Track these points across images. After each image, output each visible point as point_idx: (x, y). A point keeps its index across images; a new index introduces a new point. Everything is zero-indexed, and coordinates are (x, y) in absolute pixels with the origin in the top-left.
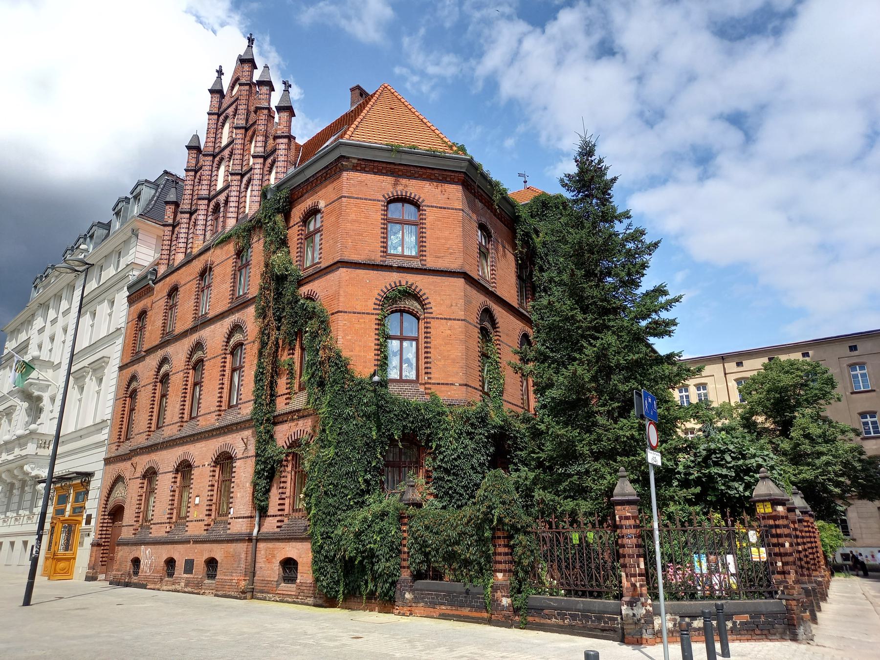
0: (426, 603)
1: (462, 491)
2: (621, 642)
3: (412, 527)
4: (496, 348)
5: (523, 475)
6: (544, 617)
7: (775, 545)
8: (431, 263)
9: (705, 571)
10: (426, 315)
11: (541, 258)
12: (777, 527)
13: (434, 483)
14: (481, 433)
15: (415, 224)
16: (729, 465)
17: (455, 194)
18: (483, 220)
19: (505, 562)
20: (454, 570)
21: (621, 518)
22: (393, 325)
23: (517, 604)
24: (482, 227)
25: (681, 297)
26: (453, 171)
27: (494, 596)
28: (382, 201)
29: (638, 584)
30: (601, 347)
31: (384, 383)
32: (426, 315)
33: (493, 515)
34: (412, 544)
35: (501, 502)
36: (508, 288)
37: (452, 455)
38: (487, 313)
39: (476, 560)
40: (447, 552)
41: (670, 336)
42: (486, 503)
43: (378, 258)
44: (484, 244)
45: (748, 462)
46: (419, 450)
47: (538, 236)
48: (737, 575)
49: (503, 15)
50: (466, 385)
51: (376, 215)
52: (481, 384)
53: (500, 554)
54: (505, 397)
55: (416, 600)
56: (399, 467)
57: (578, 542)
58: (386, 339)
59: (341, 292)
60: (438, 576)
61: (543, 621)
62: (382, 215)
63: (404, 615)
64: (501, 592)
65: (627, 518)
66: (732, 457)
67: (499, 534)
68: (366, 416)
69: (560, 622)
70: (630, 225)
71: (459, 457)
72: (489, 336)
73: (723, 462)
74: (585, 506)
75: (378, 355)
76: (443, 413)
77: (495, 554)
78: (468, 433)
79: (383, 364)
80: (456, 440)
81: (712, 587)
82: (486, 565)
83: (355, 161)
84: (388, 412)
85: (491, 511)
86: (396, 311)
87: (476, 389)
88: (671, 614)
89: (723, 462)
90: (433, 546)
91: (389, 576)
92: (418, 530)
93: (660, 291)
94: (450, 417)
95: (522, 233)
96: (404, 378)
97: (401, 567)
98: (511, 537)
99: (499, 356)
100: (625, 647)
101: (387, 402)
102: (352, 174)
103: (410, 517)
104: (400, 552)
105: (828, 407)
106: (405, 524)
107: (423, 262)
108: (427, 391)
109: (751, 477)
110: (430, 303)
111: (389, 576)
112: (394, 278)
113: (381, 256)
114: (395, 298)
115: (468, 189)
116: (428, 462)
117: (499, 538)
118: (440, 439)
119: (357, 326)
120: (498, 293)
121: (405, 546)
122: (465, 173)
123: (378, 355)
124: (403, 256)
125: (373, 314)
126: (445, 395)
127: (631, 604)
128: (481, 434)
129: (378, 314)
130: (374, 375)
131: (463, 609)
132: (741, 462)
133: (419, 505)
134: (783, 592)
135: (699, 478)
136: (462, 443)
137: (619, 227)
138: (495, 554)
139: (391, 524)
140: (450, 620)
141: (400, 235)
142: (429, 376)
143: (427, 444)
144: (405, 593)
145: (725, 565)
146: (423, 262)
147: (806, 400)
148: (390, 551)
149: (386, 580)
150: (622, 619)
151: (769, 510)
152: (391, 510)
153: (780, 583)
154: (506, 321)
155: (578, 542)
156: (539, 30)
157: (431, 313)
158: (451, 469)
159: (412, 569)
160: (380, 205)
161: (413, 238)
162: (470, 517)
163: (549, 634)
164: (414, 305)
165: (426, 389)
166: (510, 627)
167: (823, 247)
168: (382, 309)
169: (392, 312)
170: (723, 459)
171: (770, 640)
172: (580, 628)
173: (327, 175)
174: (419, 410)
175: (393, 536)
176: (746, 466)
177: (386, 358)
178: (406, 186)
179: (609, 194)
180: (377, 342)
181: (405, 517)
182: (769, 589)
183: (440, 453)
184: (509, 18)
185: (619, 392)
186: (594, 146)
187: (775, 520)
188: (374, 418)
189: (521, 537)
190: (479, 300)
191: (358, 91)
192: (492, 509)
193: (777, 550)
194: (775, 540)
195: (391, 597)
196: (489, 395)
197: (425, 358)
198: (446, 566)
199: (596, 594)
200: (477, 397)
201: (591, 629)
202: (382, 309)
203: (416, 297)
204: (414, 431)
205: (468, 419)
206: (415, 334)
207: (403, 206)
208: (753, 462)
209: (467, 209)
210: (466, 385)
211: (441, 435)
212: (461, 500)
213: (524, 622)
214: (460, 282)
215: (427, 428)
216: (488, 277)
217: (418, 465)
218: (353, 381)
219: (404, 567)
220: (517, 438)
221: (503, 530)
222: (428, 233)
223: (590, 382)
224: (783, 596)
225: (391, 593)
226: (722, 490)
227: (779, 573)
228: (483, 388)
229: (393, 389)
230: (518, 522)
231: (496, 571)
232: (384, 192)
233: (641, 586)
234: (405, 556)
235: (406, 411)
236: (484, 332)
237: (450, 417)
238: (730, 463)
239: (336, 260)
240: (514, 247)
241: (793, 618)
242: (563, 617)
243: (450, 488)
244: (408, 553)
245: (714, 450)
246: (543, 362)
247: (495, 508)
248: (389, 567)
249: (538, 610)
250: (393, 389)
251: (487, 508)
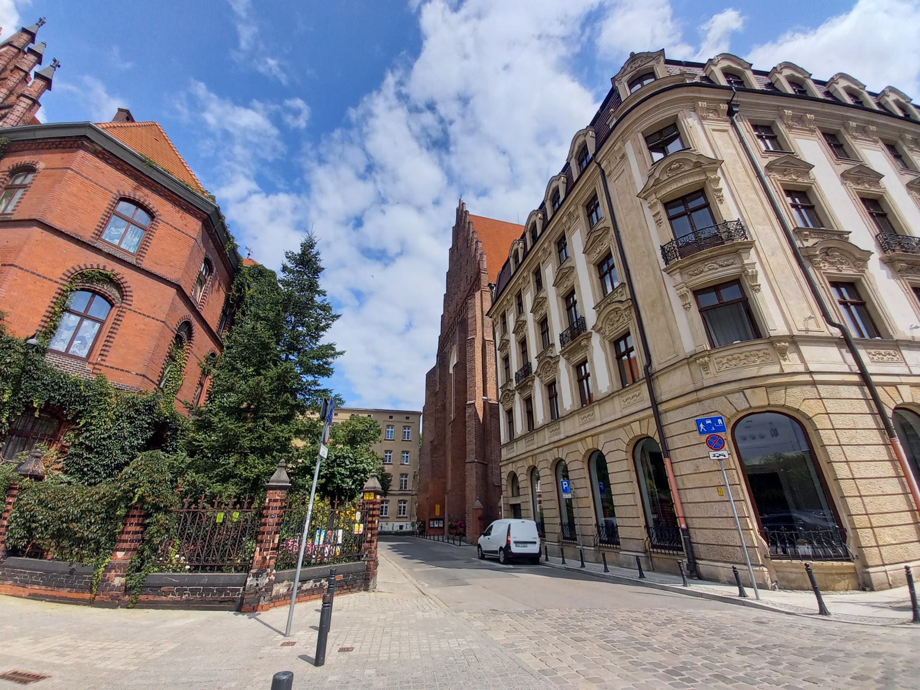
1: (101, 470)
2: (237, 611)
3: (21, 500)
4: (185, 355)
6: (159, 595)
7: (369, 522)
9: (321, 543)
10: (123, 305)
11: (246, 306)
14: (145, 420)
15: (144, 229)
16: (347, 467)
17: (194, 226)
18: (210, 257)
24: (207, 261)
25: (344, 352)
26: (198, 208)
27: (105, 576)
29: (268, 557)
30: (285, 370)
33: (135, 494)
34: (16, 517)
35: (149, 482)
36: (212, 316)
38: (187, 325)
39: (94, 539)
41: (329, 377)
43: (87, 237)
44: (204, 273)
45: (358, 466)
46: (60, 424)
47: (249, 290)
50: (144, 376)
51: (103, 203)
52: (159, 379)
53: (128, 533)
54: (178, 396)
56: (28, 438)
58: (64, 310)
59: (25, 249)
61: (157, 598)
64: (116, 572)
65: (276, 501)
66: (350, 462)
67: (135, 512)
69: (177, 598)
71: (109, 437)
73: (343, 465)
76: (107, 394)
77: (122, 532)
78: (129, 417)
79: (50, 331)
80: (112, 421)
81: (323, 555)
84: (35, 379)
85: (133, 489)
87: (153, 382)
88: (288, 580)
89: (343, 465)
90: (43, 522)
92: (28, 504)
93: (330, 347)
94: (113, 399)
95: (238, 282)
98: (148, 515)
99: (186, 362)
100: (240, 616)
101: (38, 369)
102: (89, 156)
103: (22, 489)
105: (374, 445)
106: (14, 496)
107: (139, 261)
108: (95, 371)
109: (359, 476)
110: (132, 296)
112: (101, 261)
113: (92, 237)
114: (92, 278)
116: (67, 437)
117: (134, 516)
118: (92, 417)
122: (208, 215)
126: (113, 380)
127: (256, 575)
128: (143, 420)
129: (64, 285)
130: (33, 337)
133: (39, 478)
134: (367, 555)
136: (119, 425)
137: (318, 299)
138: (122, 532)
142: (103, 358)
145: (336, 537)
146: (139, 261)
147: (366, 439)
150: (244, 589)
151: (372, 498)
154: (201, 339)
157: (130, 305)
158: (96, 447)
160: (110, 197)
162: (104, 494)
163: (161, 611)
164: (114, 293)
167: (377, 368)
168: (71, 282)
169: (83, 290)
170: (344, 462)
172: (198, 602)
173: (60, 144)
176: (357, 468)
177: (55, 327)
179: (318, 275)
182: (359, 554)
183: (87, 430)
186: (316, 243)
187: (374, 505)
190: (184, 312)
191: (125, 115)
192: (136, 488)
194: (370, 519)
196: (163, 391)
200: (151, 389)
201: (209, 602)
202: (71, 282)
203: (118, 286)
204: (62, 404)
205: (134, 405)
206: (102, 317)
207: (137, 209)
209: (199, 241)
210: (144, 376)
212: (95, 478)
216: (199, 299)
217: (52, 439)
221: (141, 508)
223: (267, 393)
224: (367, 559)
226: (338, 483)
228: (160, 384)
229: (49, 359)
230: (162, 502)
233: (271, 558)
235: (59, 383)
236: (178, 338)
237: (113, 399)
238: (348, 465)
239: (32, 217)
240: (229, 289)
242: (181, 592)
243: (87, 465)
245: (340, 456)
246: (230, 371)
247: (140, 486)
249: (155, 588)
250: (49, 359)
251: (130, 486)
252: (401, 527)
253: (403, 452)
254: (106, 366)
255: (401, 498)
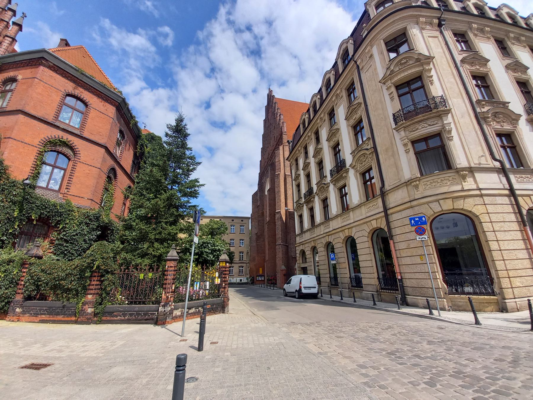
0: (31, 314)
1: (74, 252)
5: (117, 246)
7: (223, 278)
8: (86, 135)
9: (198, 289)
10: (75, 159)
11: (146, 158)
12: (226, 271)
13: (56, 247)
15: (82, 113)
17: (111, 110)
18: (123, 129)
19: (95, 289)
20: (58, 294)
21: (168, 267)
22: (50, 157)
23: (98, 311)
24: (121, 132)
25: (205, 184)
26: (113, 99)
27: (83, 308)
28: (63, 92)
29: (169, 297)
31: (34, 187)
32: (75, 159)
33: (94, 265)
37: (72, 233)
38: (113, 170)
39: (75, 289)
40: (54, 284)
42: (91, 258)
43: (50, 119)
45: (216, 248)
48: (209, 290)
49: (137, 76)
50: (92, 200)
51: (57, 98)
54: (112, 211)
55: (24, 313)
57: (142, 278)
58: (43, 163)
60: (43, 298)
61: (112, 318)
62: (61, 99)
63: (13, 321)
64: (88, 305)
67: (96, 274)
68: (12, 202)
69: (123, 318)
70: (191, 153)
71: (77, 234)
72: (111, 181)
74: (147, 261)
75: (33, 170)
76: (72, 211)
77: (89, 285)
78: (86, 223)
79: (36, 175)
82: (81, 291)
83: (52, 65)
84: (31, 203)
86: (54, 151)
90: (45, 281)
91: (6, 298)
92: (35, 272)
93: (196, 181)
96: (49, 187)
97: (16, 293)
98: (103, 276)
102: (46, 70)
104: (18, 284)
106: (26, 268)
107: (82, 133)
108: (64, 198)
111: (6, 298)
112: (60, 133)
115: (119, 112)
116: (54, 235)
117: (95, 276)
118: (66, 224)
119: (21, 150)
120: (121, 164)
121: (22, 281)
122: (119, 103)
123: (33, 170)
124: (69, 125)
125: (37, 147)
126: (75, 203)
127: (164, 306)
130: (27, 179)
131: (58, 316)
132: (213, 247)
133: (40, 258)
135: (198, 252)
138: (89, 285)
139: (15, 267)
140: (47, 323)
141: (70, 114)
143: (56, 225)
144: (16, 309)
145: (205, 286)
146: (82, 133)
148: (10, 283)
149: (3, 301)
150: (158, 313)
151: (224, 265)
152: (16, 259)
153: (222, 292)
155: (142, 278)
156: (150, 90)
157: (80, 159)
158: (70, 240)
159: (25, 295)
161: (79, 120)
162: (77, 265)
165: (64, 196)
166: (89, 324)
168: (44, 146)
169: (51, 151)
171: (216, 314)
172: (134, 320)
174: (55, 206)
175: (15, 274)
177: (39, 173)
178: (82, 92)
180: (34, 163)
181: (27, 264)
183: (64, 231)
184: (139, 78)
185: (174, 215)
188: (19, 204)
189: (109, 276)
190: (110, 163)
192: (94, 261)
193: (224, 279)
194: (224, 276)
195: (5, 311)
197: (68, 180)
198: (51, 293)
199: (138, 303)
200: (97, 208)
201: (140, 320)
202: (44, 146)
204: (48, 217)
208: (217, 248)
209: (115, 119)
211: (68, 222)
213: (100, 320)
214: (103, 150)
215: (58, 217)
216: (118, 154)
217: (45, 236)
218: (8, 180)
219: (19, 293)
220: (114, 230)
221: (99, 272)
222: (89, 120)
223: (162, 208)
225: (6, 308)
227: (223, 288)
228: (101, 204)
229: (38, 191)
231: (88, 294)
232: (65, 88)
233: (171, 297)
234: (21, 287)
235: (45, 205)
237: (76, 213)
241: (224, 305)
242: (124, 315)
244: (24, 285)
248: (7, 293)
249: (111, 313)
250: (38, 191)
251: (91, 260)
252: (241, 280)
253: (241, 240)
254: (70, 195)
255: (240, 265)
